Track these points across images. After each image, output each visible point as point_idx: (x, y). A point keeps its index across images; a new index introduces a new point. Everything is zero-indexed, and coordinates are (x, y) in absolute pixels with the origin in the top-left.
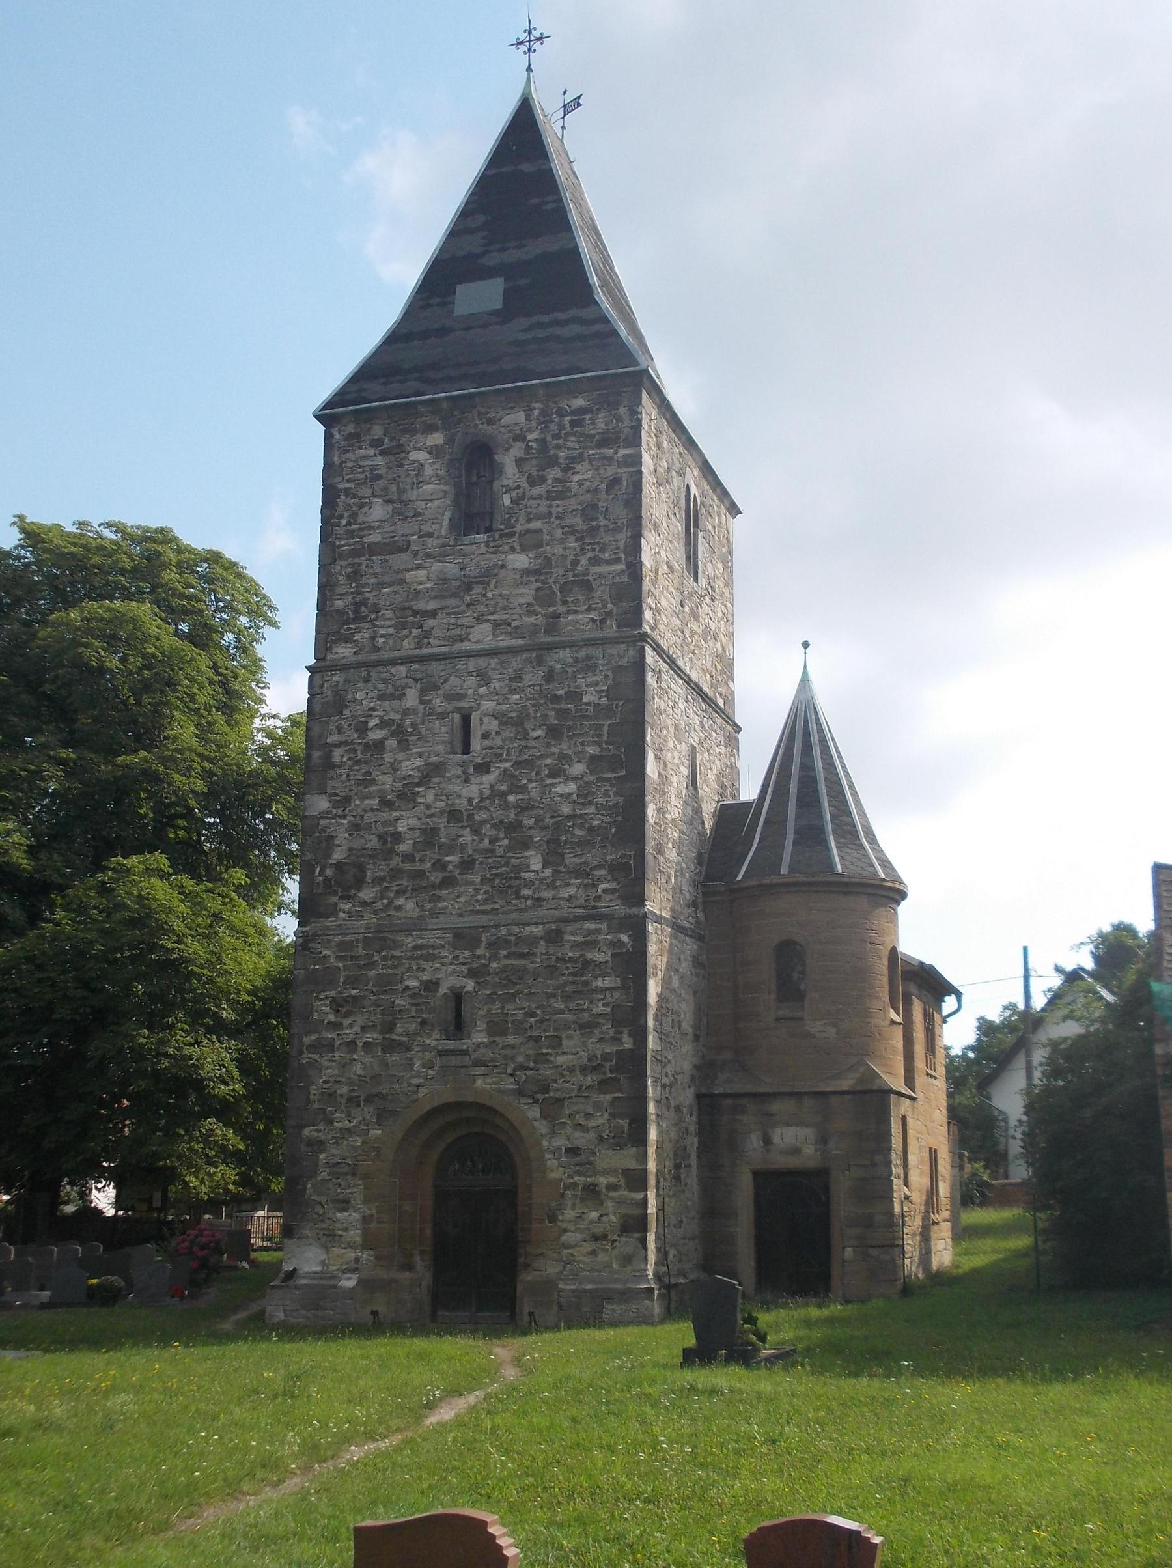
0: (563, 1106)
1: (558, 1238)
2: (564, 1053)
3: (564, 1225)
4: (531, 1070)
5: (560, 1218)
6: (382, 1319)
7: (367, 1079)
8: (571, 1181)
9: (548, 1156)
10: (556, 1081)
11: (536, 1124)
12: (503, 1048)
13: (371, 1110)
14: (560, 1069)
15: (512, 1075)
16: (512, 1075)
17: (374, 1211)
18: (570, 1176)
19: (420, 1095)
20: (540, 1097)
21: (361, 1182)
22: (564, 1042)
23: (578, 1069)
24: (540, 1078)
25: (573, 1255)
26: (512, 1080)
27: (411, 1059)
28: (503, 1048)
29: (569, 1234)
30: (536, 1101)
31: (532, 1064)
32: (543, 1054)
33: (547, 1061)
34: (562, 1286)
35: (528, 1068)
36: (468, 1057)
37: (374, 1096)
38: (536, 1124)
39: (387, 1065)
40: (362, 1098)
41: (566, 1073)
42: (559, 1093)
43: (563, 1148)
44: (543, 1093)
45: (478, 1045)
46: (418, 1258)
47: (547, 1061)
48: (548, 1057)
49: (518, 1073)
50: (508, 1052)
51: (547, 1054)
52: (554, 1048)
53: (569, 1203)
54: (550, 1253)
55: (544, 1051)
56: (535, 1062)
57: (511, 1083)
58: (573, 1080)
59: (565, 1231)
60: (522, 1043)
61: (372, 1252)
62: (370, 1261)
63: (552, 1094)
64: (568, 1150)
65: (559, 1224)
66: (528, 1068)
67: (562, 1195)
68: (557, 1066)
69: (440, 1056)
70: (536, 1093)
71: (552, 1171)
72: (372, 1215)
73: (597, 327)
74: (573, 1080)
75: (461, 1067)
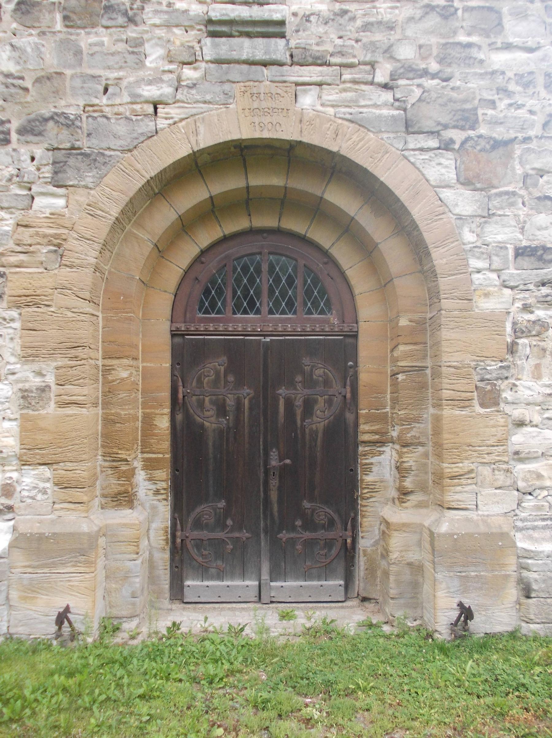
0: (510, 156)
1: (503, 442)
2: (508, 47)
3: (517, 413)
4: (434, 76)
5: (507, 395)
6: (79, 627)
7: (28, 84)
8: (532, 317)
9: (475, 263)
10: (492, 104)
11: (446, 194)
12: (367, 27)
13: (39, 152)
14: (500, 79)
15: (386, 86)
16: (386, 86)
17: (50, 379)
18: (526, 308)
19: (162, 123)
20: (457, 136)
21: (14, 313)
22: (508, 23)
23: (540, 80)
24: (454, 95)
25: (539, 476)
26: (387, 96)
27: (139, 43)
28: (367, 27)
29: (529, 429)
30: (447, 146)
31: (434, 67)
32: (459, 44)
33: (470, 61)
34: (522, 544)
35: (425, 73)
36: (281, 42)
37: (46, 120)
38: (446, 194)
39: (78, 53)
40: (14, 125)
41: (512, 87)
42: (500, 129)
43: (511, 248)
44: (462, 128)
45: (307, 18)
46: (141, 476)
47: (470, 61)
48: (474, 52)
49: (401, 82)
50: (378, 37)
51: (469, 45)
52: (486, 33)
53: (528, 365)
54: (486, 471)
55: (462, 38)
56: (441, 61)
57: (385, 104)
58: (530, 103)
59: (521, 424)
60: (411, 19)
61: (46, 471)
62: (44, 492)
63: (483, 130)
64: (520, 252)
65: (508, 409)
66: (425, 73)
67: (512, 349)
68: (493, 73)
69: (213, 35)
70: (446, 127)
71: (487, 295)
72: (44, 389)
73: (163, 173)
74: (530, 103)
75: (265, 64)
